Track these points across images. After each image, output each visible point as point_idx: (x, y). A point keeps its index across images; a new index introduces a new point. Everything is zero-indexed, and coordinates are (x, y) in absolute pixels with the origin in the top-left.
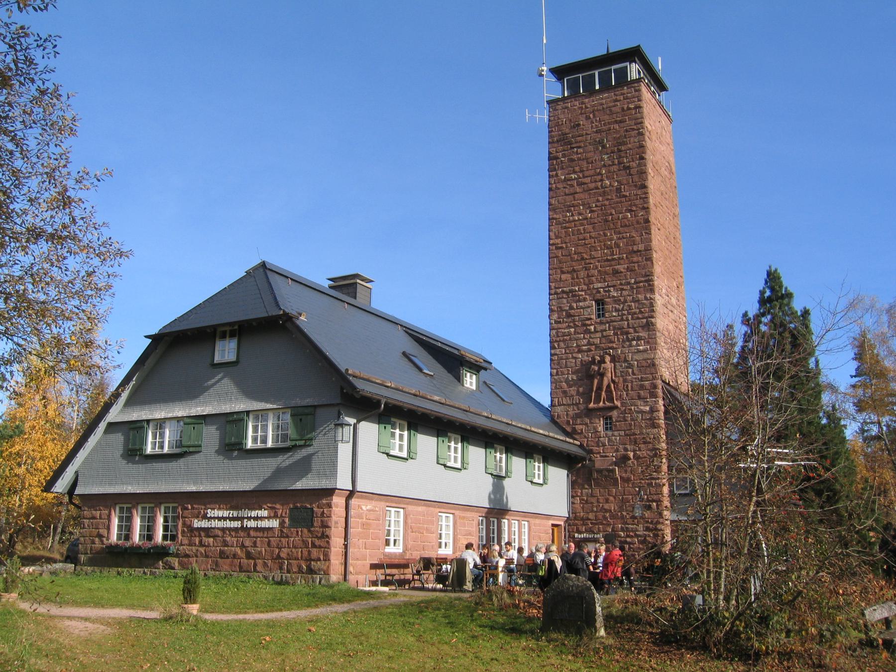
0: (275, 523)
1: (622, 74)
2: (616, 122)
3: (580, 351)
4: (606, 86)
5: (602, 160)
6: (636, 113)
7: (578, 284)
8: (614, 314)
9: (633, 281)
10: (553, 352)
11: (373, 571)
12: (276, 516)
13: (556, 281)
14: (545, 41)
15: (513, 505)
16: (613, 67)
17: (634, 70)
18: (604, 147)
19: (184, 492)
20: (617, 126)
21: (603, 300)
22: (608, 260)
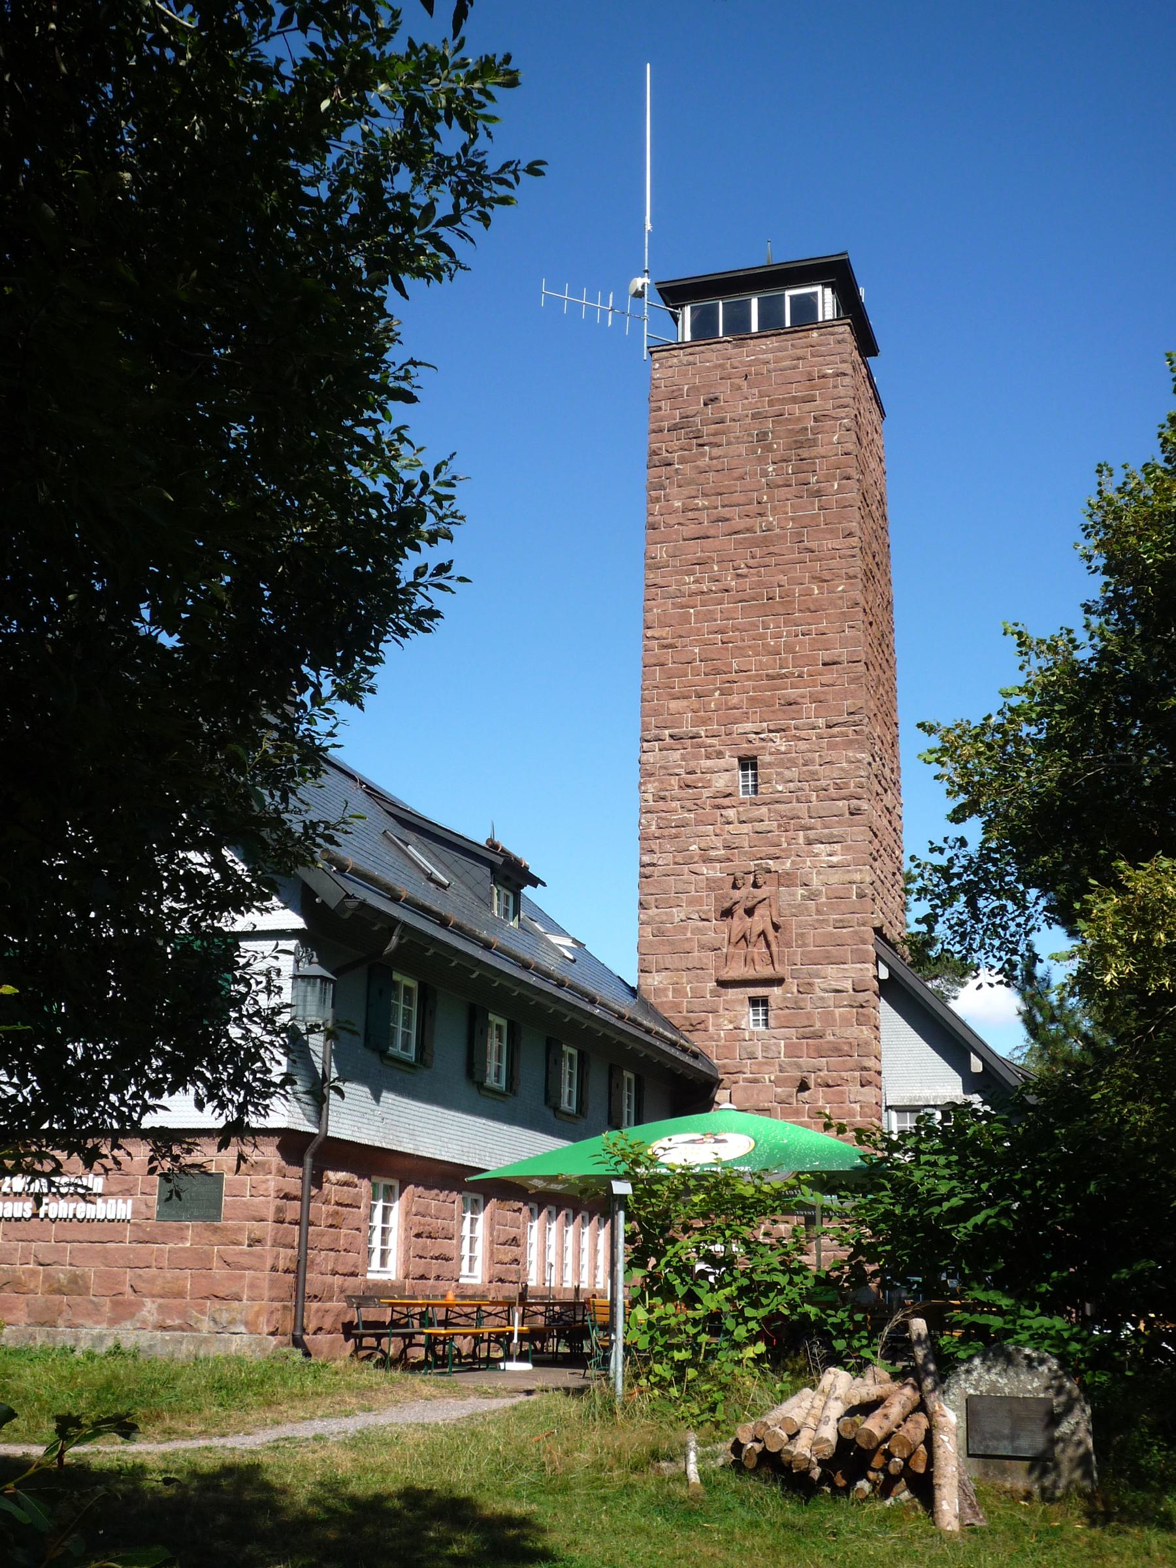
0: (120, 1208)
1: (805, 310)
2: (794, 400)
3: (708, 860)
4: (771, 321)
5: (765, 474)
6: (835, 387)
7: (704, 722)
8: (780, 788)
9: (821, 722)
10: (646, 859)
11: (780, 975)
12: (127, 1192)
13: (656, 713)
14: (648, 227)
15: (299, 32)
16: (789, 293)
17: (826, 302)
18: (768, 449)
19: (360, 1144)
20: (796, 409)
21: (755, 758)
22: (770, 677)
